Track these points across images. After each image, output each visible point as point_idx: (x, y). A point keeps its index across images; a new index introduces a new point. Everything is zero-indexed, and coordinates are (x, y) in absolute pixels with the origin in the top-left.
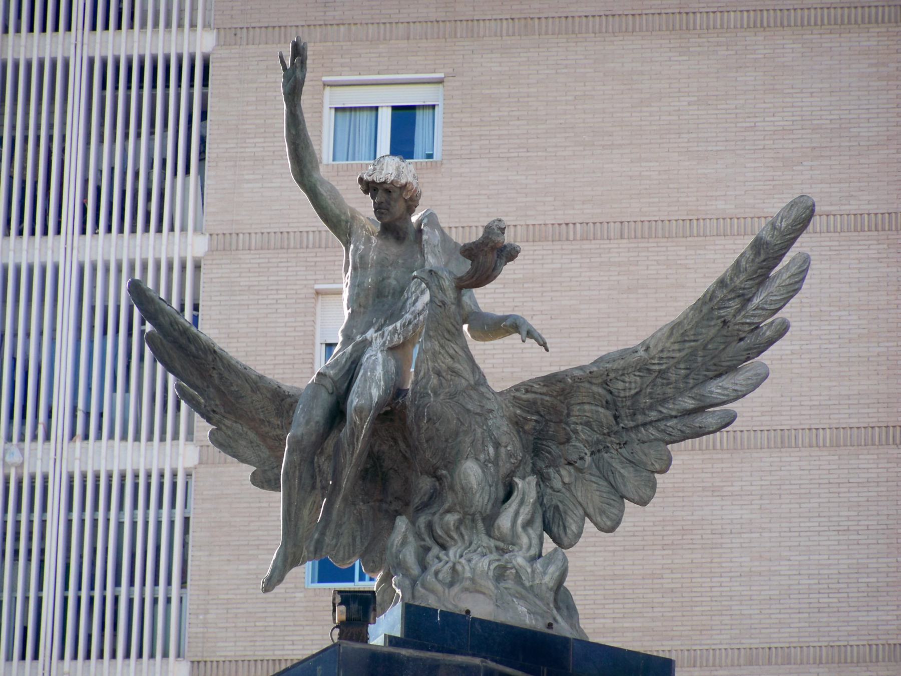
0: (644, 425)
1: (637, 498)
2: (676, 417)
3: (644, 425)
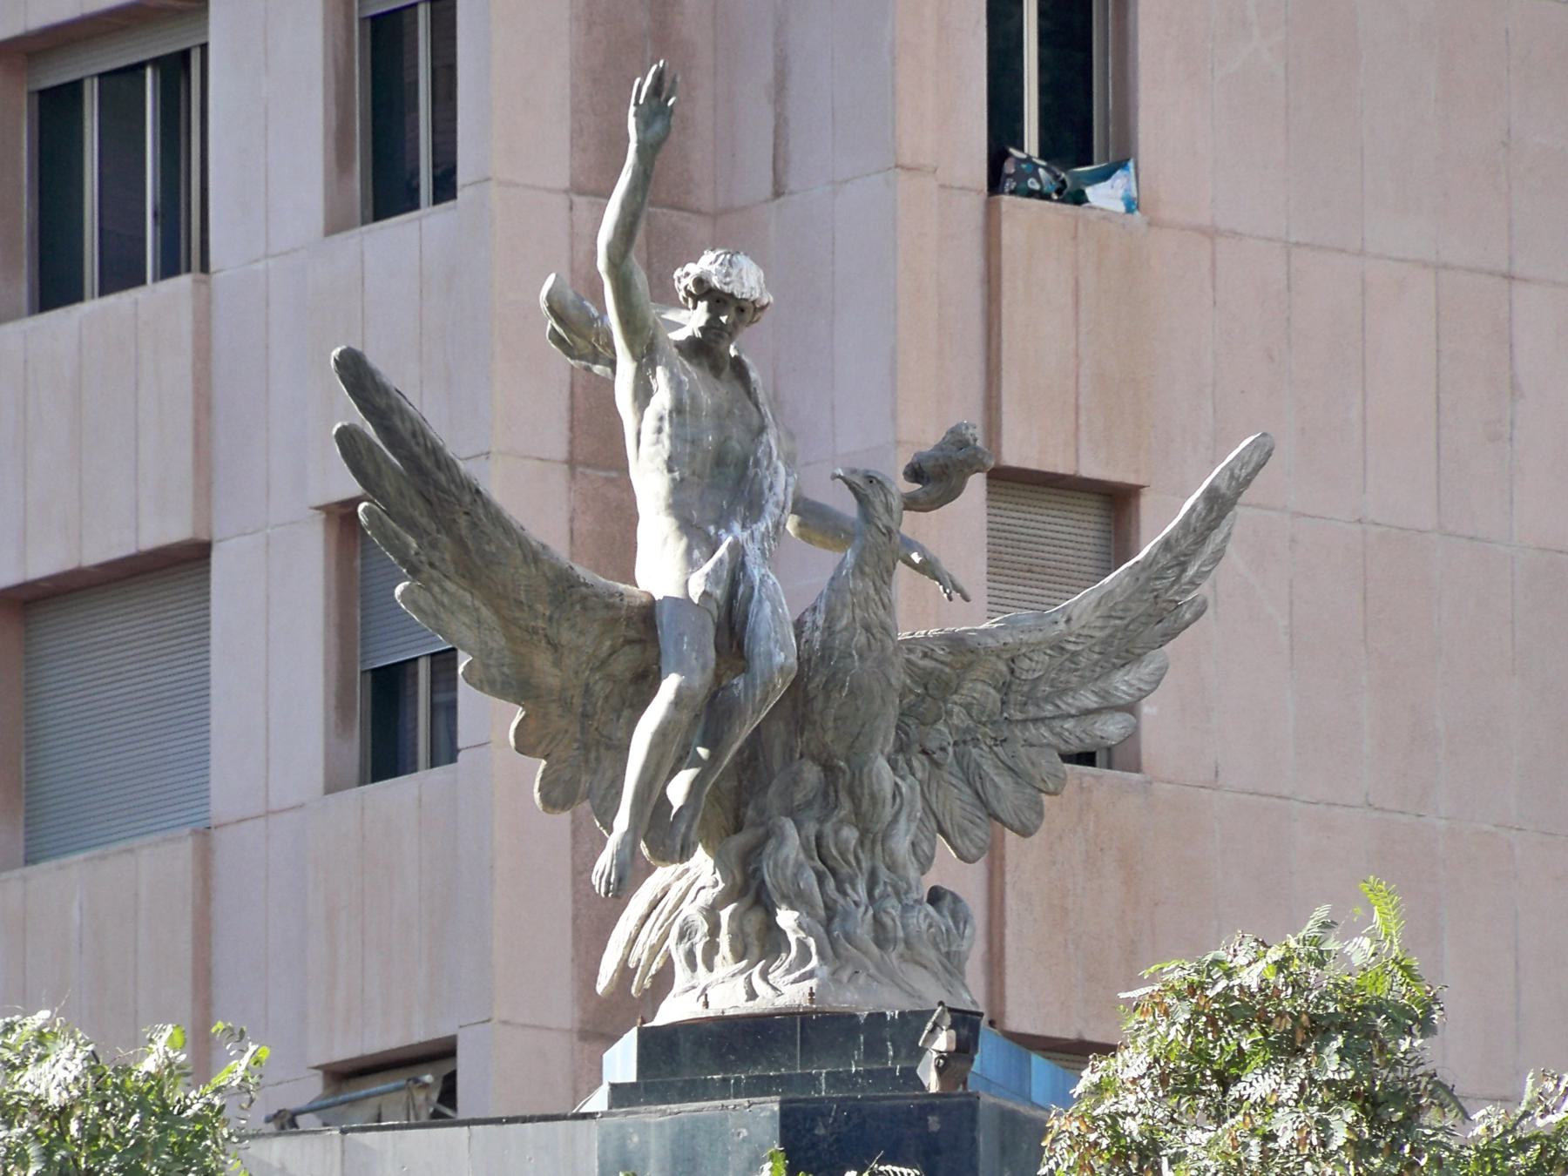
0: (1035, 720)
1: (1017, 824)
2: (1073, 716)
3: (1035, 720)
